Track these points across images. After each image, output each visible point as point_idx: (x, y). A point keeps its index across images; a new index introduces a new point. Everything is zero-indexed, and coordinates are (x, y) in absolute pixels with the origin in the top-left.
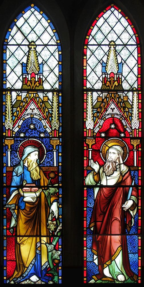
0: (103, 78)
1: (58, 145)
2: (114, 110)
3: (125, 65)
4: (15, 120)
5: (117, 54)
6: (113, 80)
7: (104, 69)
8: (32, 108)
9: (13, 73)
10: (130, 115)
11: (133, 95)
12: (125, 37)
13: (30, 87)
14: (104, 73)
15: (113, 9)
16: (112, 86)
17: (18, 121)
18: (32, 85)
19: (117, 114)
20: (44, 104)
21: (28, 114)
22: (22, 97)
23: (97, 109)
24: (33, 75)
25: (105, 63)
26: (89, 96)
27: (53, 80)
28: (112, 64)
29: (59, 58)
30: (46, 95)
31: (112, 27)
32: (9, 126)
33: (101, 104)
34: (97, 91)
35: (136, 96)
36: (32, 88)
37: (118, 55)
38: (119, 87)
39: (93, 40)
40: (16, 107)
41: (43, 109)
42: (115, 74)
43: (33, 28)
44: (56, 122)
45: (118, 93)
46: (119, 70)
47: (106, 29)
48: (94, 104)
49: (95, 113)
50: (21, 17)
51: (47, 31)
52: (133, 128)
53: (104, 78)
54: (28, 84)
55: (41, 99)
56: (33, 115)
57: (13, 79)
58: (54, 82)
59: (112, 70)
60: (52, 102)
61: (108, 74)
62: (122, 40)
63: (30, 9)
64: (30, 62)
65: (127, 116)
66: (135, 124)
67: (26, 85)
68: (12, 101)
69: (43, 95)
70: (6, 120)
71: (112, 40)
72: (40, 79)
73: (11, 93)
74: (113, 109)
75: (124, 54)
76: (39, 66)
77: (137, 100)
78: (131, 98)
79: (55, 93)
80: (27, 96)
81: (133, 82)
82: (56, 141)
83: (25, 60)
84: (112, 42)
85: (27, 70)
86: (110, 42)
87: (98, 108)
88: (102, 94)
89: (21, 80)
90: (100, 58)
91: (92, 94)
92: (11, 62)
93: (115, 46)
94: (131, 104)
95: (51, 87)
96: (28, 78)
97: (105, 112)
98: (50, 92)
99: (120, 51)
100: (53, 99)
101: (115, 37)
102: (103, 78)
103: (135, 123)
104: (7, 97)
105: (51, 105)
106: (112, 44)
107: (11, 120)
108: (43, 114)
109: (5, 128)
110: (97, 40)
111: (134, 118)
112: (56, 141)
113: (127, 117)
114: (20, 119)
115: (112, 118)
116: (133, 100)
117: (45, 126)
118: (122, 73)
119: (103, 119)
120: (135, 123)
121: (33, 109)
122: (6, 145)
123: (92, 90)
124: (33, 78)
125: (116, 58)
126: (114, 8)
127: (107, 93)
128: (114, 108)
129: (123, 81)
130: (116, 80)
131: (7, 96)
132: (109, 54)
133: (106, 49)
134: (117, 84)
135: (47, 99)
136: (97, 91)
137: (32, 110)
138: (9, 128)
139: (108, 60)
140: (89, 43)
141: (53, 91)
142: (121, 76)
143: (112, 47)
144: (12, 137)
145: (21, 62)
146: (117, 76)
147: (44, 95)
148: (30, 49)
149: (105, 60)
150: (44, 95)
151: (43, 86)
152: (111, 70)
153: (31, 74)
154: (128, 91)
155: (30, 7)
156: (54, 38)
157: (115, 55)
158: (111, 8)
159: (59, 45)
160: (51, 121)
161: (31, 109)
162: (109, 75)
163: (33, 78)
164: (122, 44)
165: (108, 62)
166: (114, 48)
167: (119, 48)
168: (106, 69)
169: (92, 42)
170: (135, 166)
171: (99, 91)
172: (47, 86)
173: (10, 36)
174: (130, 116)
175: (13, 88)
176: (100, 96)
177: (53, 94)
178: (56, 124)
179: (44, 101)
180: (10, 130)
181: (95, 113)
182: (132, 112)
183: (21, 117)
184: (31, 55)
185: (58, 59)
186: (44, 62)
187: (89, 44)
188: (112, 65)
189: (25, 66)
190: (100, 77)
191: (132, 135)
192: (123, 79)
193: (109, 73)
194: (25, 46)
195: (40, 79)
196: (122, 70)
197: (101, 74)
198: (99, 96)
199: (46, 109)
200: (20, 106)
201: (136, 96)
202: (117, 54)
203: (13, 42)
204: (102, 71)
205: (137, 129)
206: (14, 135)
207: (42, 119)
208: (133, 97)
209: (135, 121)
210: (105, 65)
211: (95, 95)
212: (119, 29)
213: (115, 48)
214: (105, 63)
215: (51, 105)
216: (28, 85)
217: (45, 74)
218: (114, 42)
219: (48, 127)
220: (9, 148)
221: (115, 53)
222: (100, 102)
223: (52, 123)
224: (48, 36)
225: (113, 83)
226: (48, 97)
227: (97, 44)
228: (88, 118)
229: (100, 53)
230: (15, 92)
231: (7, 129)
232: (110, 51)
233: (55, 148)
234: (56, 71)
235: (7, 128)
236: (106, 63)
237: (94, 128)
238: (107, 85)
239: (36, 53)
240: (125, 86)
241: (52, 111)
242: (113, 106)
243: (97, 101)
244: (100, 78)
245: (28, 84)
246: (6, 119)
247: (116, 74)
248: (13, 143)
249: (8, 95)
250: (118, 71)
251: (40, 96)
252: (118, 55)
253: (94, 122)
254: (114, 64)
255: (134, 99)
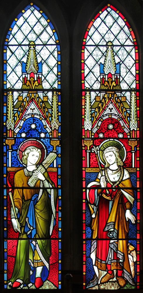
0: (23, 78)
1: (58, 146)
2: (112, 110)
3: (122, 65)
4: (16, 120)
5: (115, 54)
6: (33, 80)
7: (102, 71)
8: (33, 108)
9: (13, 73)
10: (50, 116)
11: (131, 95)
12: (122, 37)
13: (29, 87)
14: (102, 72)
15: (109, 9)
16: (110, 86)
17: (97, 122)
18: (33, 85)
19: (115, 115)
20: (44, 104)
21: (29, 115)
22: (100, 97)
23: (95, 109)
24: (32, 74)
25: (25, 63)
26: (87, 96)
27: (52, 79)
28: (110, 65)
29: (135, 57)
30: (45, 95)
31: (109, 29)
32: (10, 126)
33: (99, 104)
34: (95, 91)
35: (134, 96)
36: (31, 88)
37: (37, 54)
38: (118, 87)
39: (14, 39)
40: (17, 108)
41: (121, 109)
42: (113, 75)
43: (31, 27)
44: (56, 121)
45: (117, 93)
46: (116, 70)
47: (103, 29)
48: (15, 104)
49: (15, 113)
50: (21, 16)
51: (21, 30)
52: (131, 130)
53: (102, 79)
54: (27, 84)
55: (41, 99)
56: (34, 115)
57: (14, 79)
58: (54, 81)
59: (110, 70)
60: (130, 103)
61: (105, 75)
62: (41, 40)
63: (29, 8)
64: (29, 62)
65: (125, 116)
66: (134, 125)
67: (25, 85)
68: (13, 101)
69: (43, 94)
70: (8, 120)
71: (109, 40)
72: (39, 78)
73: (12, 93)
74: (111, 109)
75: (122, 54)
76: (37, 66)
77: (135, 100)
78: (128, 98)
79: (55, 92)
80: (28, 95)
81: (131, 81)
82: (56, 142)
83: (102, 61)
84: (32, 42)
85: (26, 69)
86: (107, 43)
87: (19, 108)
88: (100, 94)
89: (21, 81)
90: (19, 57)
91: (90, 94)
92: (12, 61)
93: (34, 46)
94: (129, 104)
95: (50, 87)
96: (27, 77)
97: (104, 111)
98: (50, 91)
99: (40, 51)
100: (53, 98)
101: (112, 37)
102: (24, 78)
103: (134, 124)
104: (9, 97)
105: (129, 105)
106: (109, 45)
107: (13, 120)
108: (44, 114)
109: (7, 128)
110: (120, 41)
111: (132, 119)
112: (56, 142)
113: (125, 118)
114: (98, 120)
115: (32, 118)
116: (131, 100)
117: (45, 126)
118: (42, 73)
119: (23, 120)
120: (134, 124)
121: (33, 109)
122: (7, 145)
123: (91, 90)
124: (32, 78)
125: (113, 58)
126: (111, 8)
127: (105, 93)
128: (112, 109)
129: (43, 80)
130: (114, 81)
131: (9, 96)
132: (29, 53)
133: (26, 48)
134: (115, 85)
135: (44, 98)
136: (95, 91)
137: (33, 110)
138: (10, 129)
139: (106, 61)
140: (10, 44)
141: (53, 90)
142: (41, 75)
143: (110, 47)
144: (91, 138)
145: (99, 63)
146: (114, 77)
147: (44, 95)
148: (30, 48)
149: (25, 60)
150: (44, 95)
151: (42, 86)
152: (108, 70)
153: (30, 74)
154: (48, 90)
155: (28, 7)
156: (53, 37)
157: (113, 55)
158: (108, 8)
159: (59, 45)
160: (51, 121)
161: (31, 109)
162: (107, 76)
163: (32, 78)
164: (94, 44)
165: (105, 63)
166: (34, 48)
167: (116, 49)
168: (104, 70)
169: (90, 42)
170: (55, 168)
171: (97, 91)
172: (46, 85)
173: (88, 36)
174: (128, 117)
175: (13, 88)
176: (98, 95)
177: (53, 93)
178: (56, 124)
179: (44, 101)
180: (12, 130)
181: (15, 113)
182: (130, 113)
183: (22, 117)
184: (30, 54)
185: (134, 58)
186: (43, 62)
187: (86, 44)
188: (110, 66)
189: (25, 66)
190: (98, 78)
191: (52, 136)
192: (43, 78)
193: (107, 74)
194: (50, 46)
195: (39, 78)
196: (42, 69)
197: (99, 75)
198: (97, 96)
199: (46, 109)
200: (21, 108)
201: (134, 96)
202: (115, 54)
203: (90, 42)
204: (100, 72)
205: (89, 131)
206: (93, 137)
207: (42, 119)
208: (131, 97)
209: (88, 123)
210: (102, 66)
211: (93, 94)
212: (115, 29)
213: (34, 48)
214: (25, 62)
215: (129, 105)
216: (27, 85)
217: (123, 74)
218: (112, 42)
219: (49, 127)
220: (88, 149)
221: (112, 53)
222: (98, 101)
223: (52, 123)
224: (48, 35)
225: (111, 83)
226: (48, 96)
227: (94, 44)
228: (86, 119)
229: (20, 53)
230: (17, 92)
231: (53, 129)
232: (107, 51)
233: (133, 149)
234: (133, 70)
235: (8, 129)
236: (27, 63)
237: (92, 129)
238: (105, 85)
239: (113, 53)
240: (124, 86)
241: (52, 110)
242: (111, 106)
243: (95, 101)
244: (122, 79)
245: (105, 85)
246: (8, 119)
247: (114, 75)
248: (14, 143)
249: (10, 95)
250: (115, 71)
251: (40, 95)
252: (37, 54)
253: (92, 122)
254: (111, 65)
255: (131, 98)
